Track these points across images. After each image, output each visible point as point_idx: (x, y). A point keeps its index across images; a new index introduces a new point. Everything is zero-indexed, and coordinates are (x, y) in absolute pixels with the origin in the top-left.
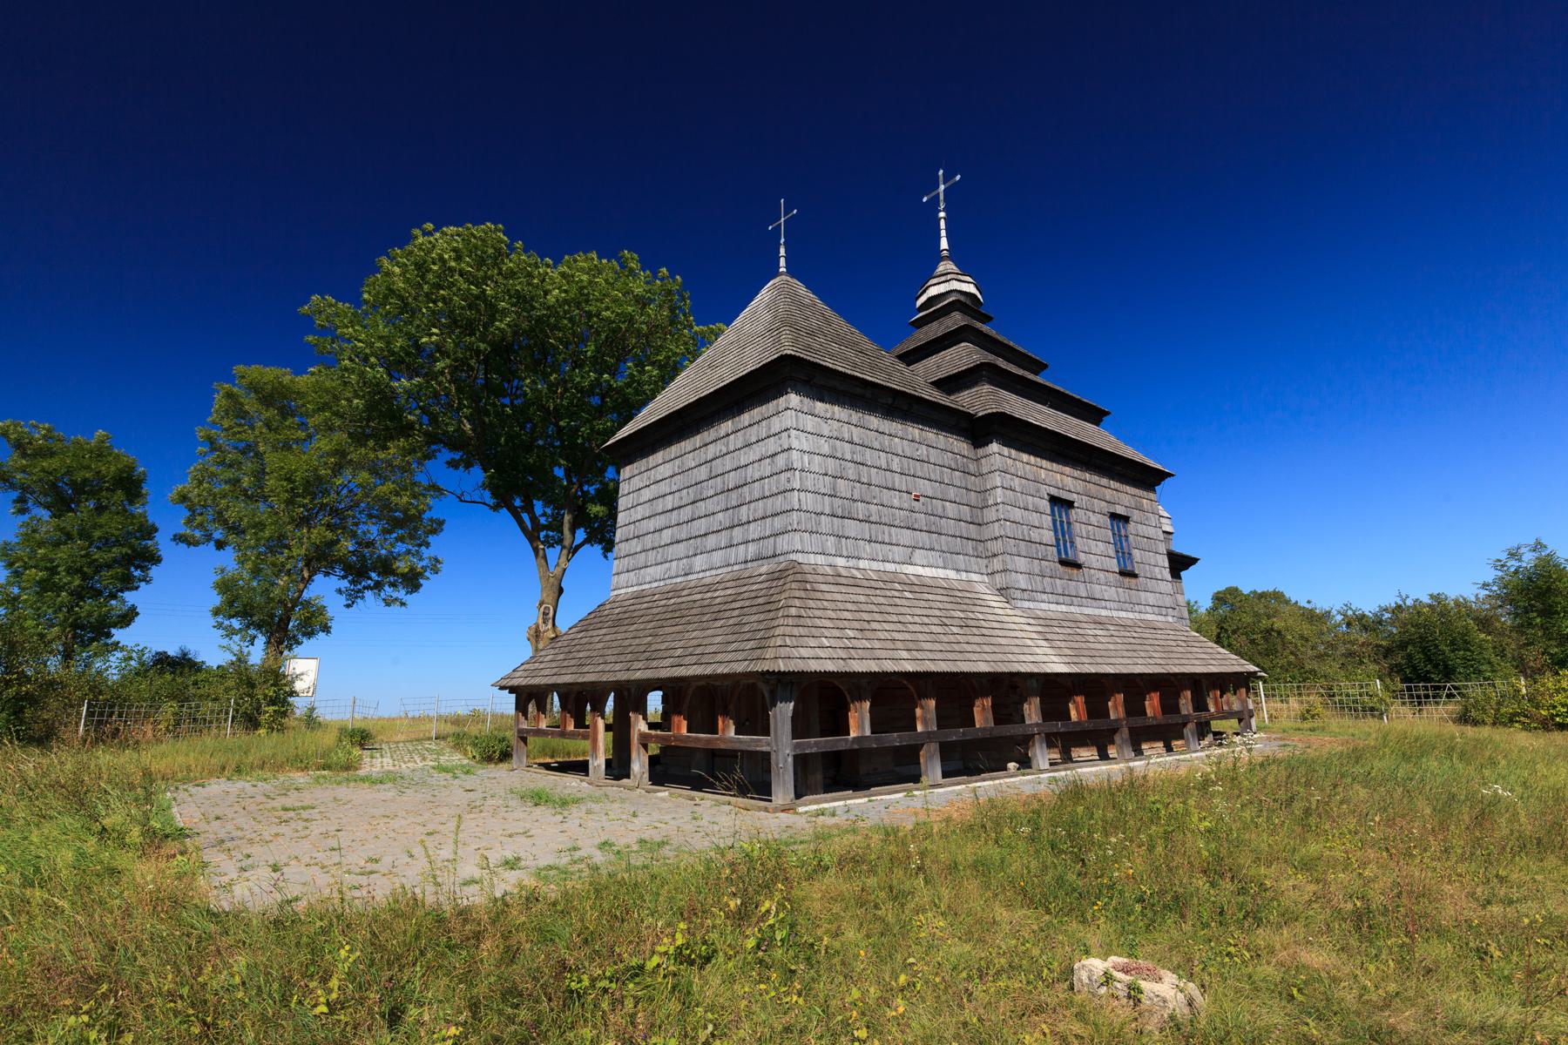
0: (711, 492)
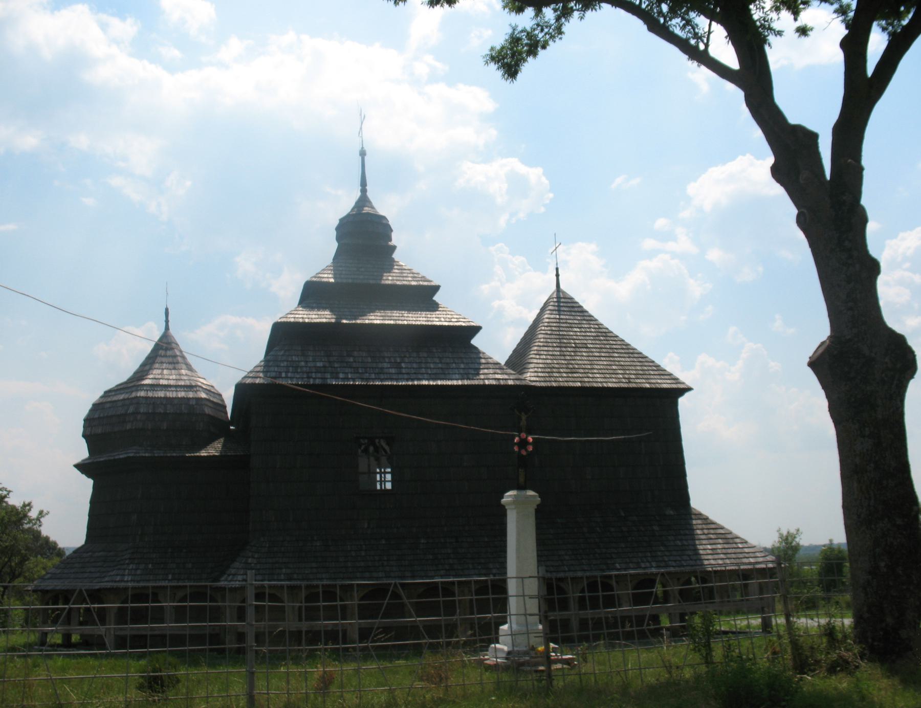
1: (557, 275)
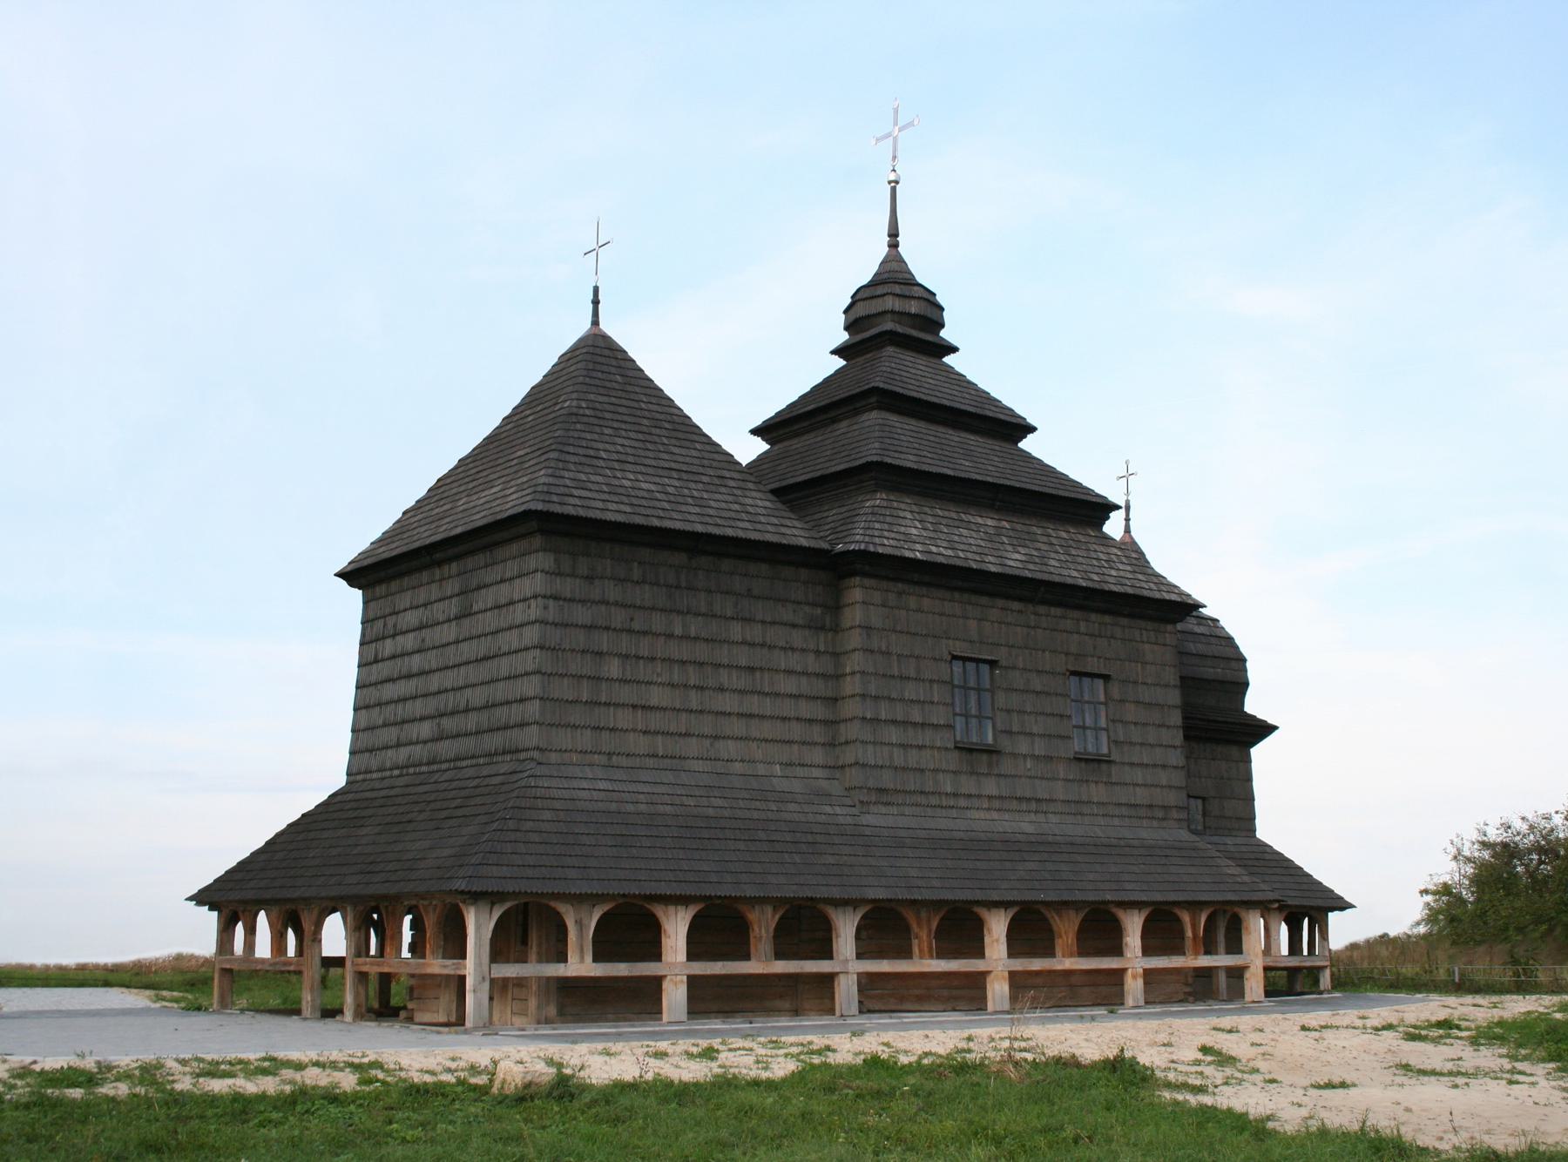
1: (596, 302)
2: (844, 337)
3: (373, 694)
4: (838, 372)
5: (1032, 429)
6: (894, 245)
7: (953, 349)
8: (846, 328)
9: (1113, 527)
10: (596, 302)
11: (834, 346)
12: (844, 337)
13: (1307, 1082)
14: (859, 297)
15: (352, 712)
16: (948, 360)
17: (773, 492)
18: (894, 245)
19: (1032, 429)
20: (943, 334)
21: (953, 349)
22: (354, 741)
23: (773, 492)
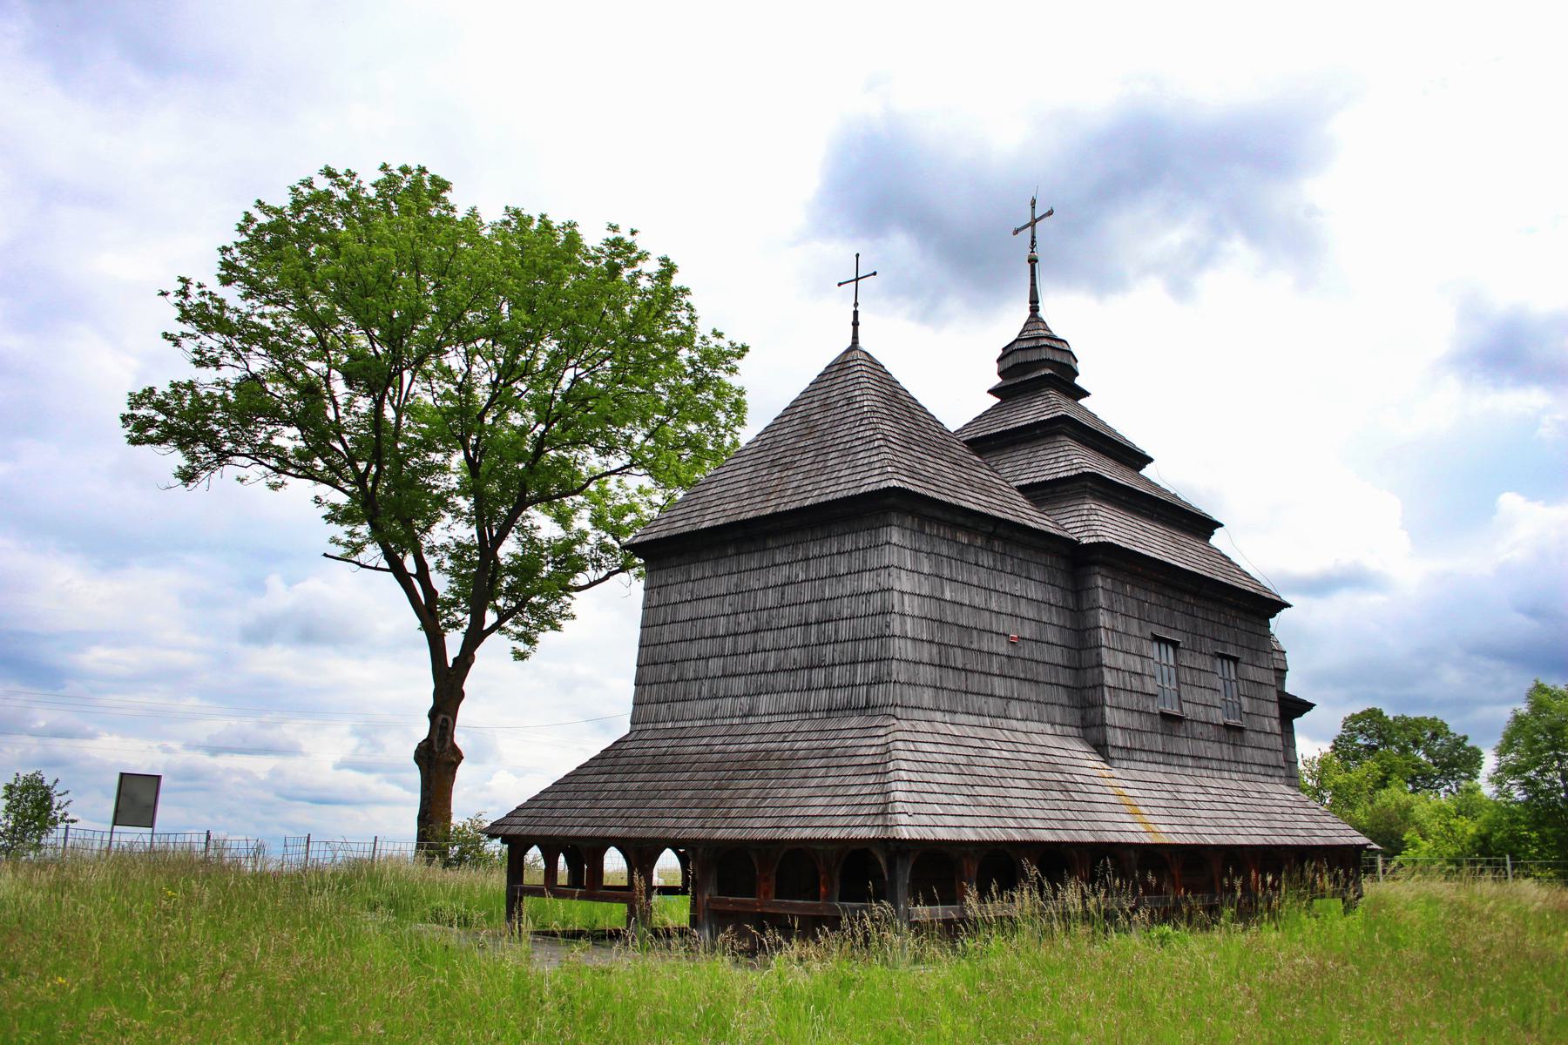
0: (784, 623)
1: (855, 324)
2: (997, 380)
3: (650, 671)
4: (994, 408)
5: (1150, 460)
6: (1034, 309)
7: (1086, 394)
8: (1000, 374)
9: (1217, 540)
10: (855, 324)
11: (991, 386)
12: (997, 380)
13: (1395, 891)
14: (1008, 351)
15: (635, 668)
16: (1082, 402)
17: (301, 753)
18: (1034, 309)
19: (1150, 460)
20: (1078, 381)
21: (1086, 394)
22: (645, 618)
23: (301, 753)
